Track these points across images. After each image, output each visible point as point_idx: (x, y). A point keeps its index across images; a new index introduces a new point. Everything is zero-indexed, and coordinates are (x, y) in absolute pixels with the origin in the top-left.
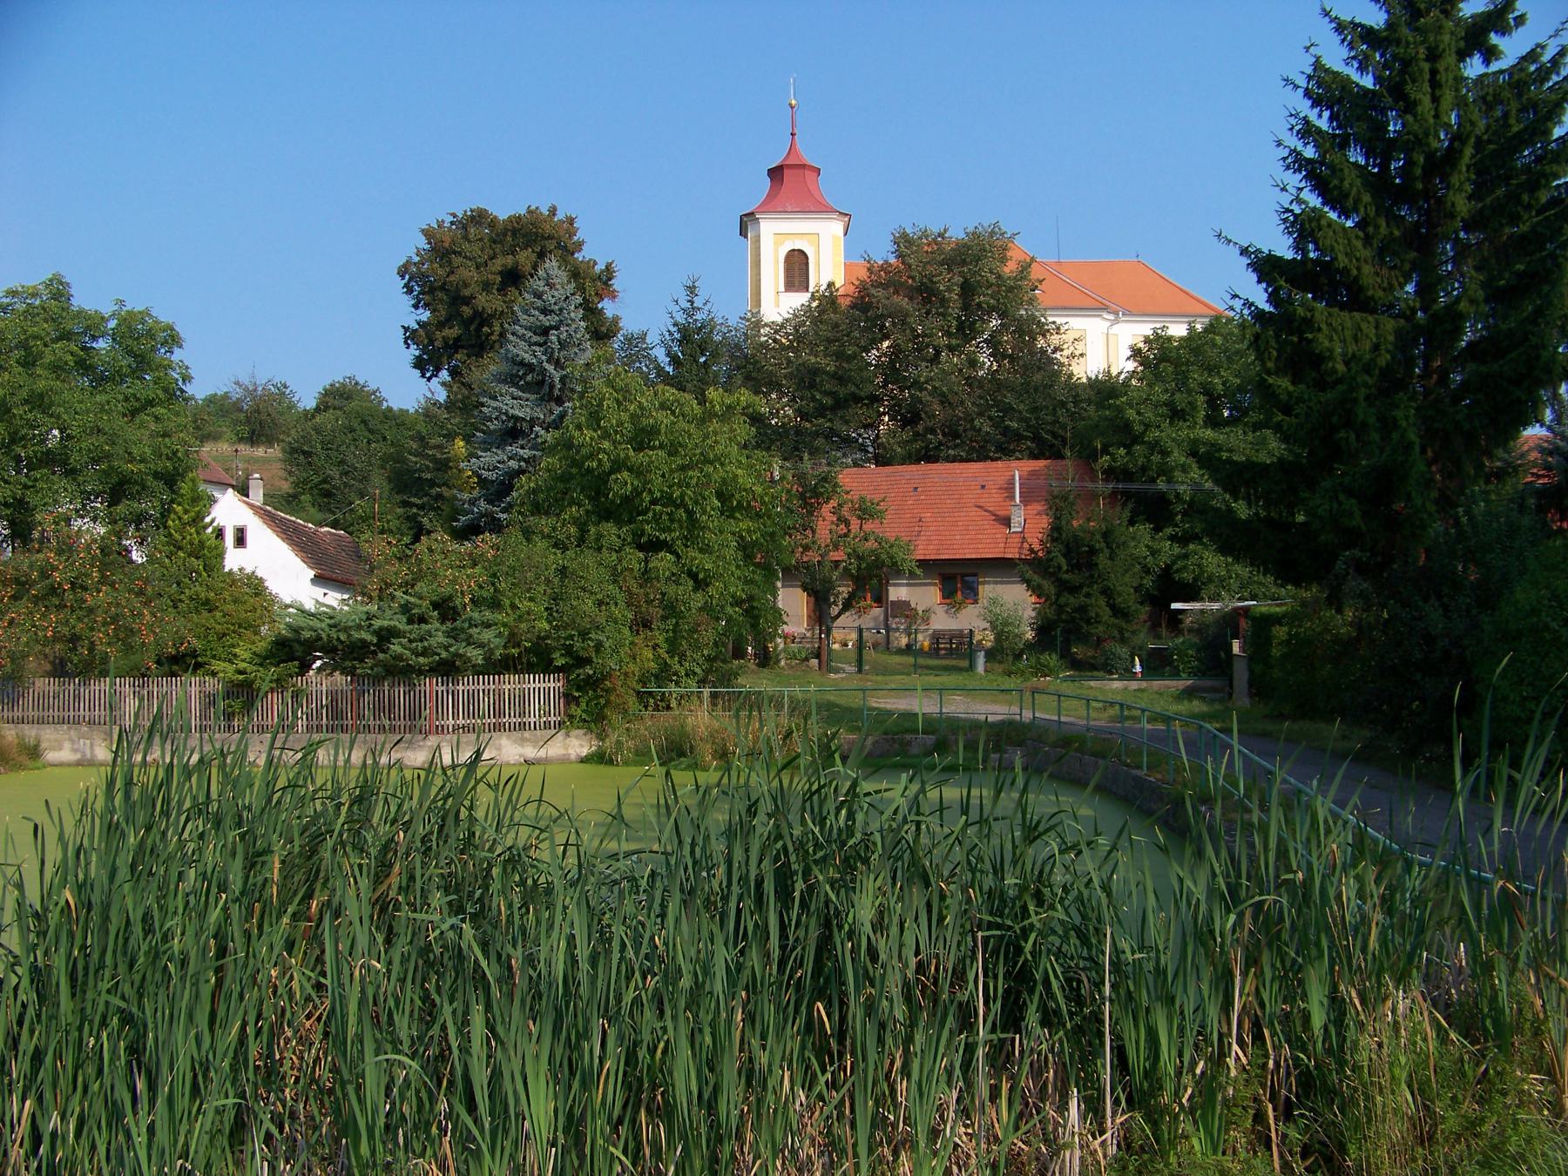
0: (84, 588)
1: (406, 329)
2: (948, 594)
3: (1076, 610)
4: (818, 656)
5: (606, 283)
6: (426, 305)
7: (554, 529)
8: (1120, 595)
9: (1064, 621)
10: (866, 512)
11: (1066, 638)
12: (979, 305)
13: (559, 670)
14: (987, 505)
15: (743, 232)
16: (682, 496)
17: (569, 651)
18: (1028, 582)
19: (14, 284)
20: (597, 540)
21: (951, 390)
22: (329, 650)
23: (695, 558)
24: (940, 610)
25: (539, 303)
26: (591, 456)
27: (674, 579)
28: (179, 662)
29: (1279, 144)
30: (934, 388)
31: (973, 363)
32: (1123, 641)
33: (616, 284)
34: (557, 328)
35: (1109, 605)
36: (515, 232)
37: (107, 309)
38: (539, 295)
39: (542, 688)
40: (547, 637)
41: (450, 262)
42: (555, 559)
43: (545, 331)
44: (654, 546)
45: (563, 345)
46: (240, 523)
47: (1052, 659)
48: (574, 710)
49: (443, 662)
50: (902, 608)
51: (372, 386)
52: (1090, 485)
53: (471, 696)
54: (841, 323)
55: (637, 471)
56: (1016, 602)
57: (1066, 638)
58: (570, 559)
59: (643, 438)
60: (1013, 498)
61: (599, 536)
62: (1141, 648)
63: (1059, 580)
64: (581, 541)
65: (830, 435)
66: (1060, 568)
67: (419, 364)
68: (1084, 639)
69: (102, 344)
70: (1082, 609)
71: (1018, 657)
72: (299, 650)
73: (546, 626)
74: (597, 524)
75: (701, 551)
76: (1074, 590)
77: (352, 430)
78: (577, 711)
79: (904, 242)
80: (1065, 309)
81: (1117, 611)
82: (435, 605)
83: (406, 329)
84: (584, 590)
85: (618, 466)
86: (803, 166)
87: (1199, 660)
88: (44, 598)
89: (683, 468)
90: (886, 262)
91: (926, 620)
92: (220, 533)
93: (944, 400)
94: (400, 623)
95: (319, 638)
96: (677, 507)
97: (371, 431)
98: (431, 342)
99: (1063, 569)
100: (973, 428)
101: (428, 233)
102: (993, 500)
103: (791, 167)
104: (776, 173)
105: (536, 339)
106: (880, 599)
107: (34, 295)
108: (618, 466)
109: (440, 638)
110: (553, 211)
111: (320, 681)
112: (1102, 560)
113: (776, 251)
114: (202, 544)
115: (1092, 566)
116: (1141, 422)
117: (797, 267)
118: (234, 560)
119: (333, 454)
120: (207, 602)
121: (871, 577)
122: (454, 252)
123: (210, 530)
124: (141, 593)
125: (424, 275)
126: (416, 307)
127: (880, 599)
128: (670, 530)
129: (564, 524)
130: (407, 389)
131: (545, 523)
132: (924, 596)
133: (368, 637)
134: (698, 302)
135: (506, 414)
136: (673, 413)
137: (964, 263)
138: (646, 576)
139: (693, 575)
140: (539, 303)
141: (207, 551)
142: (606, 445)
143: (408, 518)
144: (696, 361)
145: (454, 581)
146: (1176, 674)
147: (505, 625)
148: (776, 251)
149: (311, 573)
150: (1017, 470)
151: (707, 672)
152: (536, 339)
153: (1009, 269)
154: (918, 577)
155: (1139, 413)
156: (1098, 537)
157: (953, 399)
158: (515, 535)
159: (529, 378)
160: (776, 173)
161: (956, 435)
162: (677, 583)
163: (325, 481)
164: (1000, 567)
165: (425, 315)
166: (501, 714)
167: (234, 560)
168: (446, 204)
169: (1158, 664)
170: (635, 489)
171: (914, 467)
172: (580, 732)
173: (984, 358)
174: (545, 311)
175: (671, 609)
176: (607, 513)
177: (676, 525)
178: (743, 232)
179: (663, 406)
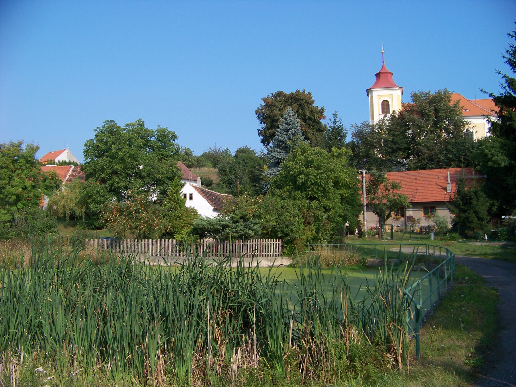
0: (139, 213)
1: (259, 130)
2: (426, 213)
3: (465, 218)
4: (378, 234)
5: (322, 114)
6: (264, 123)
7: (281, 193)
8: (480, 213)
9: (461, 222)
10: (394, 187)
11: (462, 229)
12: (440, 116)
13: (281, 237)
14: (439, 183)
15: (368, 95)
16: (320, 182)
17: (282, 231)
18: (449, 209)
19: (129, 123)
20: (294, 196)
21: (430, 146)
22: (209, 231)
23: (325, 202)
24: (423, 219)
25: (286, 122)
26: (292, 170)
27: (318, 209)
28: (169, 235)
29: (504, 57)
30: (425, 145)
31: (439, 136)
32: (482, 229)
33: (325, 114)
34: (291, 129)
35: (476, 216)
36: (291, 98)
37: (155, 128)
38: (286, 119)
39: (274, 243)
40: (276, 227)
41: (271, 109)
42: (280, 203)
43: (288, 130)
44: (312, 199)
45: (293, 135)
46: (191, 193)
47: (456, 235)
48: (285, 250)
49: (242, 235)
50: (410, 218)
51: (252, 149)
52: (470, 176)
53: (252, 246)
54: (400, 122)
55: (306, 175)
56: (446, 216)
57: (462, 229)
58: (285, 203)
59: (308, 164)
60: (447, 181)
61: (295, 195)
62: (489, 231)
63: (460, 208)
64: (290, 197)
65: (392, 161)
66: (460, 204)
67: (263, 141)
68: (469, 228)
69: (153, 139)
70: (467, 218)
71: (445, 234)
72: (199, 231)
73: (275, 224)
74: (294, 192)
75: (328, 200)
76: (464, 211)
77: (240, 163)
78: (285, 251)
79: (415, 97)
80: (477, 116)
81: (479, 219)
82: (242, 218)
83: (259, 130)
84: (288, 212)
85: (301, 173)
86: (387, 72)
87: (508, 235)
88: (128, 215)
89: (321, 173)
90: (409, 103)
91: (419, 222)
92: (185, 196)
93: (428, 149)
94: (230, 223)
95: (205, 228)
96: (319, 186)
97: (246, 163)
98: (266, 134)
99: (461, 204)
100: (438, 158)
101: (264, 100)
102: (441, 182)
103: (382, 73)
104: (378, 75)
105: (285, 133)
106: (403, 215)
107: (133, 125)
108: (301, 173)
109: (242, 227)
110: (304, 91)
111: (208, 241)
112: (474, 201)
113: (379, 101)
114: (178, 199)
115: (471, 203)
116: (491, 154)
117: (385, 105)
118: (189, 204)
119: (232, 171)
120: (179, 217)
121: (399, 208)
122: (273, 106)
123: (181, 195)
124: (155, 214)
125: (263, 113)
126: (261, 123)
127: (403, 215)
128: (318, 193)
129: (284, 192)
130: (259, 148)
131: (278, 191)
132: (418, 214)
133: (218, 227)
134: (337, 120)
135: (275, 157)
136: (318, 156)
137: (435, 102)
138: (309, 208)
139: (324, 208)
140: (286, 122)
141: (179, 202)
142: (297, 166)
143: (255, 191)
144: (337, 139)
145: (247, 210)
146: (499, 241)
147: (262, 224)
148: (379, 101)
149: (213, 208)
150: (449, 172)
151: (331, 238)
152: (285, 133)
153: (451, 104)
154: (411, 208)
155: (490, 151)
156: (472, 194)
157: (431, 148)
158: (269, 195)
159: (283, 145)
160: (378, 75)
161: (432, 160)
162: (319, 210)
163: (230, 179)
164: (441, 204)
165: (264, 126)
166: (261, 251)
167: (189, 204)
168: (269, 91)
169: (493, 237)
170: (305, 180)
171: (415, 171)
172: (287, 257)
173: (444, 134)
174: (288, 124)
175: (317, 219)
176: (298, 188)
177: (320, 192)
178: (368, 95)
179: (316, 154)
